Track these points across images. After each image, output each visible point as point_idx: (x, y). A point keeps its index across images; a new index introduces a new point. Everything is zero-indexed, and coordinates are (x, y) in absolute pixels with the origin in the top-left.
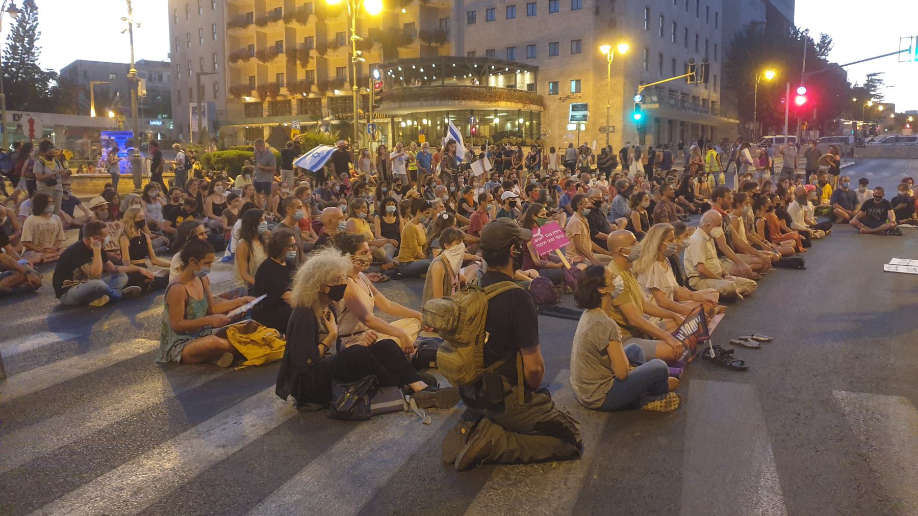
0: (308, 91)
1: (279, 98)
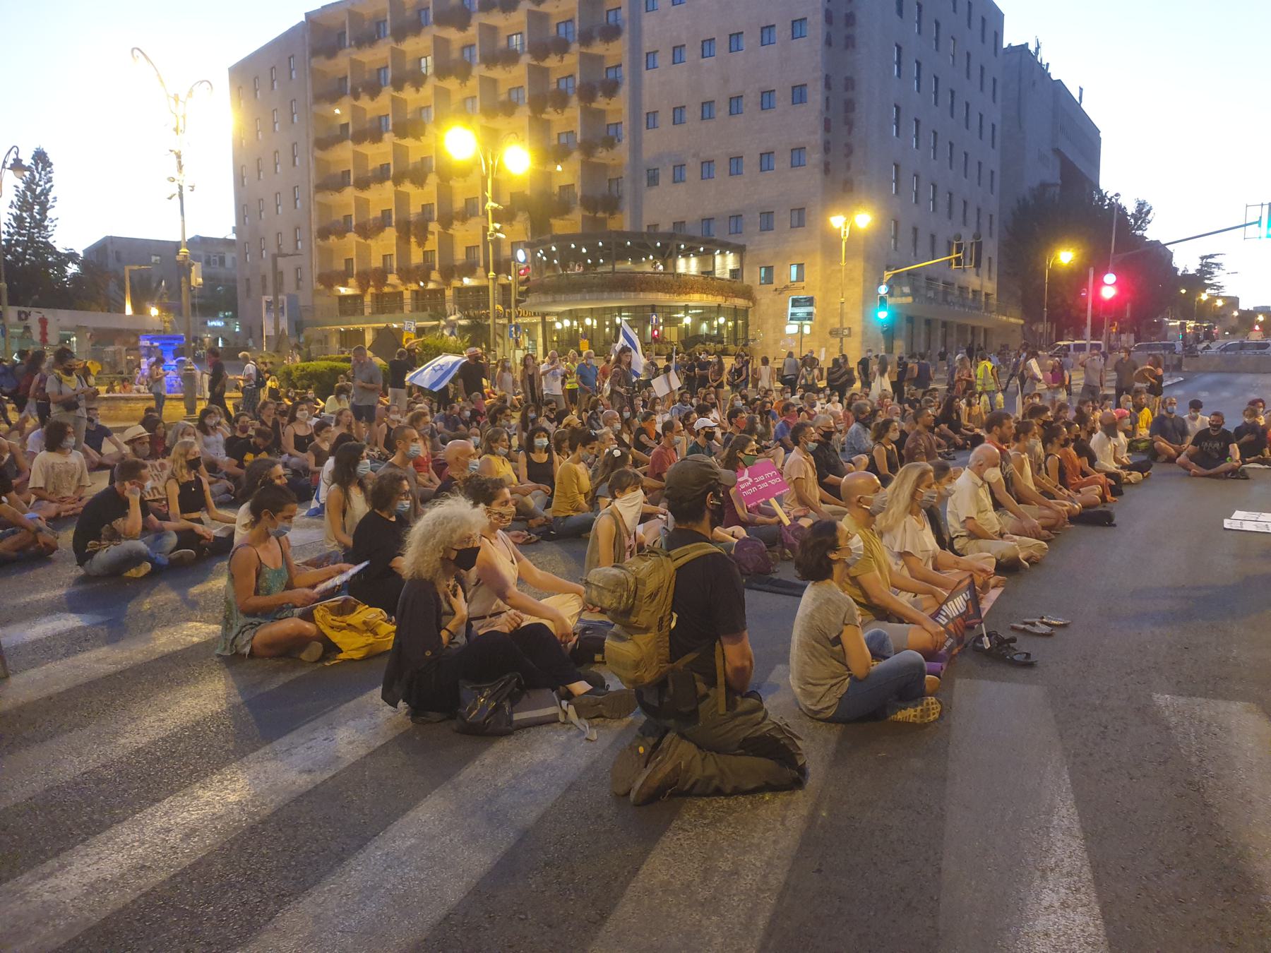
0: (427, 279)
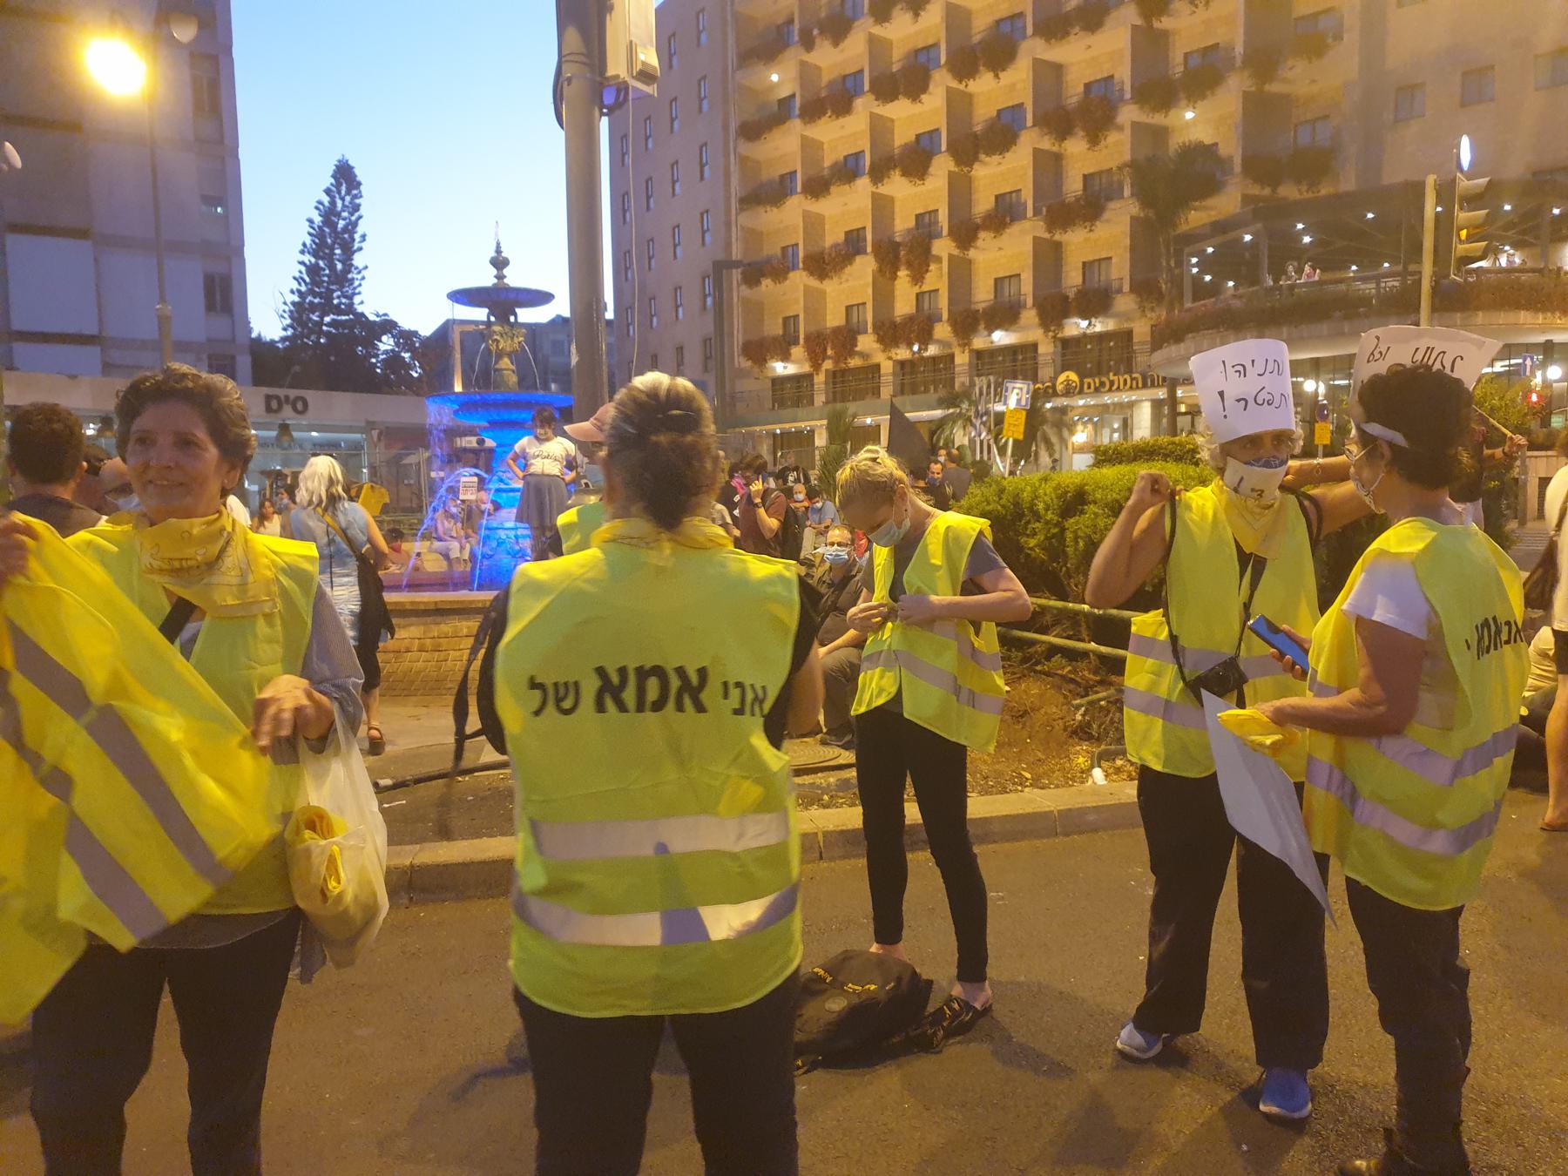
0: (926, 337)
1: (854, 362)
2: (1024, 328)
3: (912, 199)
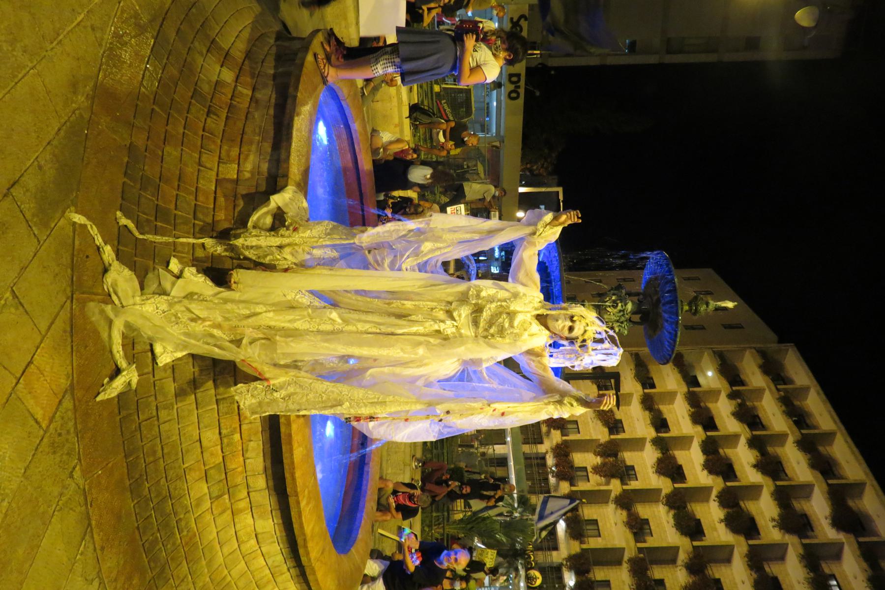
0: (561, 476)
2: (568, 543)
3: (644, 461)
